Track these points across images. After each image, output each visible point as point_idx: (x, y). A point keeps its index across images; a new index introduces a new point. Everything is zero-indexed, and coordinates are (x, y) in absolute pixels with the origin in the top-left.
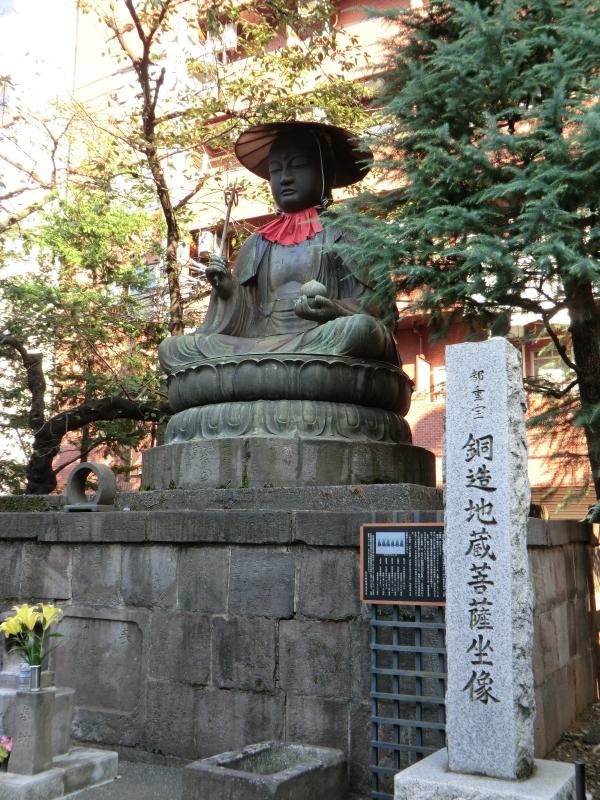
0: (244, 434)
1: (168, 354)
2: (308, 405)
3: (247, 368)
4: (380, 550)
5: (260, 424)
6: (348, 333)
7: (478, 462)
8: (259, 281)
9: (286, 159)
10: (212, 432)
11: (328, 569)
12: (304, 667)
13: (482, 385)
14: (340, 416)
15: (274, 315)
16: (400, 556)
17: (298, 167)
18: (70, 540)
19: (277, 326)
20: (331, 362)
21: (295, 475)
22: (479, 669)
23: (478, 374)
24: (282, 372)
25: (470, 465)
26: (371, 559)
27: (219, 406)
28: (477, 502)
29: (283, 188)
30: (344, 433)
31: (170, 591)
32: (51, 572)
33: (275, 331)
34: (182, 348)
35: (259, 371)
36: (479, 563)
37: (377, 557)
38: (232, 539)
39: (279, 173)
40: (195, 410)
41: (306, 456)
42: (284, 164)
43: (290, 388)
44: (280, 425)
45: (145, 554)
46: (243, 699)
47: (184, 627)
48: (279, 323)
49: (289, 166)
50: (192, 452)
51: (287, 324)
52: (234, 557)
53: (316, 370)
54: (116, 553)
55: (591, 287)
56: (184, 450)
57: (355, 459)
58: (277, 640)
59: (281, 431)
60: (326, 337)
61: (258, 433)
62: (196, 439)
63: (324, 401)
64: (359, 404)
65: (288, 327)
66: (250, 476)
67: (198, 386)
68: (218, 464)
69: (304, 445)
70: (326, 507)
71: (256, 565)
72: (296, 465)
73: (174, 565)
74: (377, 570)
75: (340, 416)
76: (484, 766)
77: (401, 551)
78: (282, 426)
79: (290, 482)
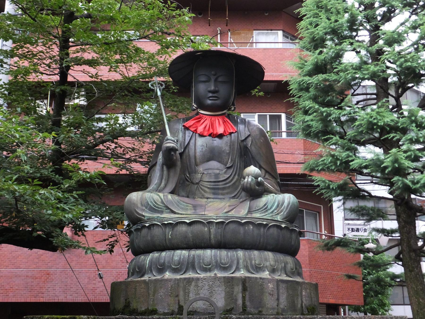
0: (232, 273)
1: (139, 205)
2: (270, 255)
5: (244, 266)
6: (288, 206)
9: (214, 75)
19: (205, 191)
20: (243, 221)
21: (276, 304)
24: (256, 231)
30: (289, 274)
33: (203, 195)
34: (151, 202)
35: (241, 229)
39: (207, 84)
40: (185, 253)
41: (281, 291)
43: (260, 243)
44: (257, 267)
48: (206, 189)
49: (216, 80)
50: (200, 285)
51: (213, 191)
53: (274, 231)
56: (193, 284)
57: (304, 293)
59: (257, 272)
60: (271, 208)
64: (226, 249)
65: (214, 194)
66: (248, 303)
67: (190, 235)
68: (223, 295)
69: (280, 283)
72: (276, 297)
78: (258, 269)
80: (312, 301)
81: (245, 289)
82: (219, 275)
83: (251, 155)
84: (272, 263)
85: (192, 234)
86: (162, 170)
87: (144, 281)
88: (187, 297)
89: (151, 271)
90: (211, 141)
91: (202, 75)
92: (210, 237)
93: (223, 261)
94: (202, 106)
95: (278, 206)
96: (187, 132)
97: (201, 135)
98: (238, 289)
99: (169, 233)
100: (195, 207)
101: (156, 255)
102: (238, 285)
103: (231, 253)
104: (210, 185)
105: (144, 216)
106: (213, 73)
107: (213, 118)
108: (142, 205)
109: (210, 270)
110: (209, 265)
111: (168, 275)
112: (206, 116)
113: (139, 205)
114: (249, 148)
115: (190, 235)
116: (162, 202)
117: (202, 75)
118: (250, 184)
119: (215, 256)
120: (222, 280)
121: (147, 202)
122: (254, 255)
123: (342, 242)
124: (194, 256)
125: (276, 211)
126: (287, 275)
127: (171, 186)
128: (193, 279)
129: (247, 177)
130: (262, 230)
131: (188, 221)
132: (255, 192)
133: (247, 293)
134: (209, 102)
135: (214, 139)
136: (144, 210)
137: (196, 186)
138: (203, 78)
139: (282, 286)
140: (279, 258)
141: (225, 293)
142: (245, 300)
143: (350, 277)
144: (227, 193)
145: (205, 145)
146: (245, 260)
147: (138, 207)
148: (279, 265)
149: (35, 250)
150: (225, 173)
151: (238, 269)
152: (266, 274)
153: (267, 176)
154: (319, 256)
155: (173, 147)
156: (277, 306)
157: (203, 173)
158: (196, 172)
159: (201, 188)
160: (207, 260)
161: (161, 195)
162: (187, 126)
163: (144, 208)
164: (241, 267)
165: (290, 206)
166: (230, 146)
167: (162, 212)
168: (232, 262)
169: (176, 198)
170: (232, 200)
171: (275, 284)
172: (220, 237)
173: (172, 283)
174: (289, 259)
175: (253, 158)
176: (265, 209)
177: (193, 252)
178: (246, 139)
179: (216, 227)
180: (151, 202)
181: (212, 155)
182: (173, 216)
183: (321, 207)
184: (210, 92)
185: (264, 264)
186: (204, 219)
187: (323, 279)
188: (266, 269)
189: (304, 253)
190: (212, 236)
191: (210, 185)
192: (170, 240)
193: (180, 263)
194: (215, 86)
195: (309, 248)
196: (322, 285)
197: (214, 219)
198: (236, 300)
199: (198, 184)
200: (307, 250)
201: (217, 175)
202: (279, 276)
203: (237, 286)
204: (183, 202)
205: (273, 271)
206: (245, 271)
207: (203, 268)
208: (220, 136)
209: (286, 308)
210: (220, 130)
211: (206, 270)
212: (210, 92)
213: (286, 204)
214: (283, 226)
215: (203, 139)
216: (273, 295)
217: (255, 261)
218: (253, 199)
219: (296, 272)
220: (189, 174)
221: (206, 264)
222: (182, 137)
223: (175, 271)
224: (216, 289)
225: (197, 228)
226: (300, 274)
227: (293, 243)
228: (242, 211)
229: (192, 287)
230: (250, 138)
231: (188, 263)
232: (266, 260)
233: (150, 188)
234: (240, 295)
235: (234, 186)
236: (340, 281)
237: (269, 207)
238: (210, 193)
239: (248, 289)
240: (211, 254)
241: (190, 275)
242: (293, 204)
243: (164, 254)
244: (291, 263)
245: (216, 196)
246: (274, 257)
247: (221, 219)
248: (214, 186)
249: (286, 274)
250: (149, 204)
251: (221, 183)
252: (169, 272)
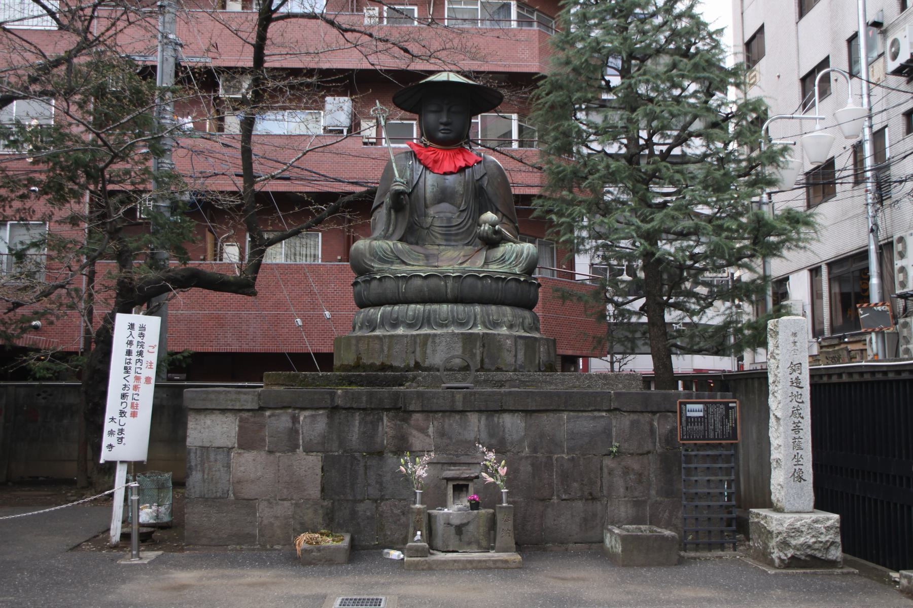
1: (368, 255)
2: (508, 310)
4: (689, 414)
7: (795, 375)
11: (633, 423)
12: (619, 483)
13: (796, 339)
15: (433, 228)
16: (701, 417)
18: (534, 408)
19: (436, 238)
22: (797, 467)
23: (795, 334)
24: (494, 285)
25: (792, 376)
26: (684, 419)
28: (795, 393)
31: (521, 441)
32: (414, 432)
35: (479, 283)
36: (796, 421)
37: (688, 418)
38: (505, 408)
40: (420, 307)
44: (494, 323)
45: (499, 418)
46: (579, 504)
47: (532, 465)
50: (437, 341)
52: (569, 419)
53: (513, 285)
54: (473, 418)
56: (430, 340)
58: (601, 469)
65: (446, 240)
66: (486, 360)
67: (426, 289)
70: (589, 387)
71: (585, 423)
73: (524, 425)
74: (687, 425)
76: (800, 509)
77: (701, 414)
78: (496, 324)
82: (456, 331)
84: (510, 318)
86: (389, 214)
87: (377, 337)
89: (383, 326)
99: (403, 286)
100: (427, 257)
101: (388, 308)
103: (469, 308)
109: (446, 326)
111: (401, 331)
113: (368, 255)
115: (426, 289)
116: (392, 252)
119: (452, 311)
124: (429, 311)
126: (525, 331)
127: (399, 233)
128: (430, 335)
130: (500, 283)
131: (423, 275)
132: (492, 242)
134: (440, 135)
136: (373, 261)
138: (434, 108)
144: (461, 240)
146: (482, 316)
150: (458, 216)
151: (475, 325)
152: (504, 330)
153: (504, 221)
158: (426, 215)
160: (443, 316)
161: (390, 243)
167: (392, 263)
168: (469, 317)
169: (407, 247)
170: (466, 248)
174: (527, 314)
175: (489, 200)
177: (428, 307)
178: (482, 178)
181: (444, 195)
182: (404, 268)
184: (442, 124)
190: (449, 290)
193: (415, 317)
199: (428, 228)
205: (511, 327)
211: (442, 326)
212: (442, 124)
213: (525, 255)
214: (522, 279)
218: (489, 249)
223: (410, 326)
225: (433, 282)
226: (537, 329)
227: (531, 296)
228: (477, 264)
230: (486, 177)
232: (504, 315)
233: (376, 233)
235: (469, 232)
241: (425, 331)
242: (532, 255)
243: (396, 308)
245: (448, 243)
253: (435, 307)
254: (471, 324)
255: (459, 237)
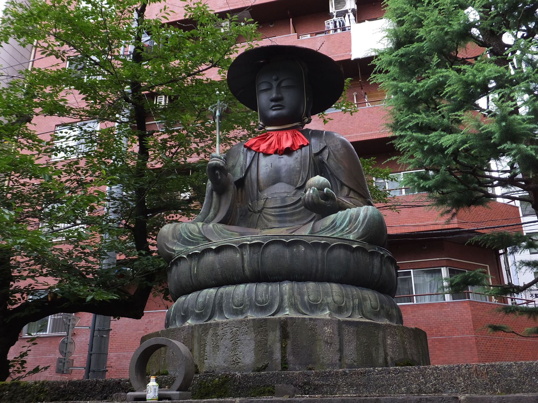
0: (273, 315)
1: (170, 238)
2: (335, 287)
3: (273, 249)
5: (291, 304)
6: (364, 220)
8: (246, 182)
9: (276, 80)
10: (236, 313)
14: (365, 299)
15: (265, 210)
17: (287, 87)
19: (269, 220)
21: (337, 357)
24: (310, 254)
27: (242, 286)
29: (273, 104)
30: (368, 315)
34: (186, 233)
35: (287, 252)
39: (269, 92)
40: (212, 291)
41: (346, 338)
42: (275, 84)
44: (311, 305)
50: (220, 332)
51: (279, 219)
53: (340, 253)
55: (147, 237)
56: (211, 332)
59: (312, 312)
60: (341, 225)
61: (288, 313)
62: (217, 319)
63: (347, 284)
65: (280, 222)
66: (290, 358)
68: (252, 345)
69: (344, 326)
72: (338, 346)
75: (365, 299)
78: (314, 307)
79: (333, 365)
80: (405, 352)
81: (285, 336)
83: (330, 171)
84: (337, 298)
85: (219, 264)
88: (202, 352)
90: (277, 160)
91: (265, 82)
92: (243, 267)
93: (259, 298)
94: (268, 121)
95: (350, 221)
96: (249, 154)
97: (266, 154)
98: (274, 336)
102: (274, 330)
103: (273, 287)
104: (275, 212)
105: (174, 251)
106: (274, 77)
107: (280, 133)
108: (174, 238)
109: (242, 312)
110: (241, 305)
112: (273, 132)
113: (170, 238)
114: (326, 162)
115: (218, 266)
116: (200, 232)
117: (265, 82)
118: (312, 196)
120: (251, 324)
121: (180, 233)
122: (307, 288)
123: (470, 277)
124: (222, 294)
125: (348, 229)
126: (364, 316)
127: (221, 215)
129: (309, 189)
130: (320, 251)
131: (214, 247)
133: (289, 342)
134: (274, 113)
135: (281, 156)
136: (175, 244)
137: (258, 215)
139: (348, 332)
140: (350, 293)
141: (256, 343)
142: (285, 353)
143: (496, 328)
144: (298, 220)
145: (270, 165)
146: (292, 296)
147: (168, 241)
148: (349, 302)
149: (122, 319)
150: (295, 194)
152: (326, 314)
153: (352, 194)
154: (487, 320)
155: (216, 164)
156: (340, 360)
157: (267, 198)
159: (264, 217)
162: (248, 145)
163: (176, 241)
164: (286, 305)
165: (367, 220)
166: (301, 161)
171: (336, 327)
172: (256, 266)
173: (185, 333)
176: (332, 228)
177: (222, 290)
179: (250, 252)
180: (186, 233)
183: (487, 267)
184: (272, 100)
185: (322, 300)
186: (235, 243)
187: (494, 347)
188: (327, 308)
189: (468, 317)
191: (275, 212)
192: (197, 275)
193: (205, 306)
194: (278, 92)
195: (472, 310)
196: (493, 353)
197: (248, 241)
198: (272, 353)
199: (260, 212)
200: (470, 313)
201: (283, 199)
202: (349, 317)
203: (273, 331)
204: (228, 230)
206: (292, 311)
207: (234, 310)
208: (289, 152)
209: (355, 364)
210: (287, 144)
213: (361, 218)
215: (268, 158)
216: (331, 343)
217: (309, 296)
219: (382, 312)
220: (252, 203)
221: (236, 304)
222: (243, 159)
224: (242, 338)
225: (226, 255)
229: (209, 336)
230: (327, 151)
231: (214, 306)
232: (326, 294)
234: (278, 345)
236: (517, 349)
237: (338, 224)
238: (275, 221)
239: (291, 336)
240: (245, 290)
244: (372, 299)
245: (282, 225)
246: (342, 290)
247: (257, 240)
248: (279, 212)
249: (363, 315)
250: (181, 235)
251: (289, 208)
252: (193, 319)
253: (230, 289)
254: (276, 307)
255: (295, 218)
